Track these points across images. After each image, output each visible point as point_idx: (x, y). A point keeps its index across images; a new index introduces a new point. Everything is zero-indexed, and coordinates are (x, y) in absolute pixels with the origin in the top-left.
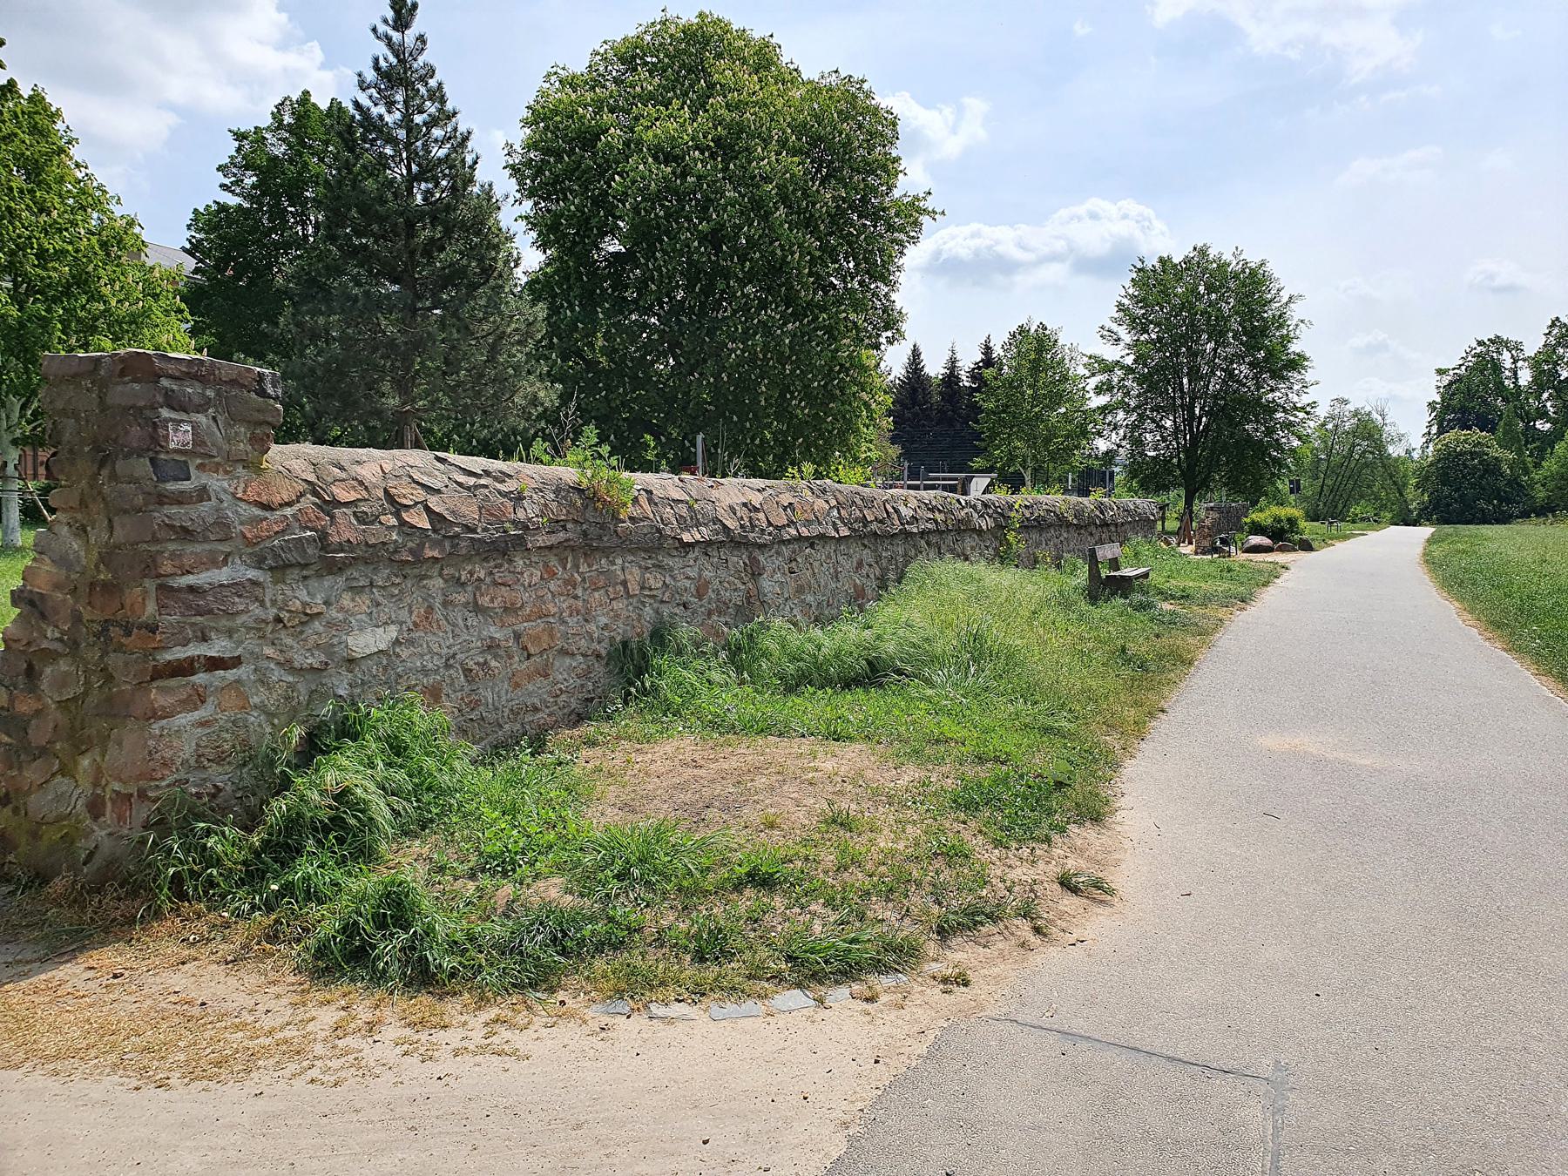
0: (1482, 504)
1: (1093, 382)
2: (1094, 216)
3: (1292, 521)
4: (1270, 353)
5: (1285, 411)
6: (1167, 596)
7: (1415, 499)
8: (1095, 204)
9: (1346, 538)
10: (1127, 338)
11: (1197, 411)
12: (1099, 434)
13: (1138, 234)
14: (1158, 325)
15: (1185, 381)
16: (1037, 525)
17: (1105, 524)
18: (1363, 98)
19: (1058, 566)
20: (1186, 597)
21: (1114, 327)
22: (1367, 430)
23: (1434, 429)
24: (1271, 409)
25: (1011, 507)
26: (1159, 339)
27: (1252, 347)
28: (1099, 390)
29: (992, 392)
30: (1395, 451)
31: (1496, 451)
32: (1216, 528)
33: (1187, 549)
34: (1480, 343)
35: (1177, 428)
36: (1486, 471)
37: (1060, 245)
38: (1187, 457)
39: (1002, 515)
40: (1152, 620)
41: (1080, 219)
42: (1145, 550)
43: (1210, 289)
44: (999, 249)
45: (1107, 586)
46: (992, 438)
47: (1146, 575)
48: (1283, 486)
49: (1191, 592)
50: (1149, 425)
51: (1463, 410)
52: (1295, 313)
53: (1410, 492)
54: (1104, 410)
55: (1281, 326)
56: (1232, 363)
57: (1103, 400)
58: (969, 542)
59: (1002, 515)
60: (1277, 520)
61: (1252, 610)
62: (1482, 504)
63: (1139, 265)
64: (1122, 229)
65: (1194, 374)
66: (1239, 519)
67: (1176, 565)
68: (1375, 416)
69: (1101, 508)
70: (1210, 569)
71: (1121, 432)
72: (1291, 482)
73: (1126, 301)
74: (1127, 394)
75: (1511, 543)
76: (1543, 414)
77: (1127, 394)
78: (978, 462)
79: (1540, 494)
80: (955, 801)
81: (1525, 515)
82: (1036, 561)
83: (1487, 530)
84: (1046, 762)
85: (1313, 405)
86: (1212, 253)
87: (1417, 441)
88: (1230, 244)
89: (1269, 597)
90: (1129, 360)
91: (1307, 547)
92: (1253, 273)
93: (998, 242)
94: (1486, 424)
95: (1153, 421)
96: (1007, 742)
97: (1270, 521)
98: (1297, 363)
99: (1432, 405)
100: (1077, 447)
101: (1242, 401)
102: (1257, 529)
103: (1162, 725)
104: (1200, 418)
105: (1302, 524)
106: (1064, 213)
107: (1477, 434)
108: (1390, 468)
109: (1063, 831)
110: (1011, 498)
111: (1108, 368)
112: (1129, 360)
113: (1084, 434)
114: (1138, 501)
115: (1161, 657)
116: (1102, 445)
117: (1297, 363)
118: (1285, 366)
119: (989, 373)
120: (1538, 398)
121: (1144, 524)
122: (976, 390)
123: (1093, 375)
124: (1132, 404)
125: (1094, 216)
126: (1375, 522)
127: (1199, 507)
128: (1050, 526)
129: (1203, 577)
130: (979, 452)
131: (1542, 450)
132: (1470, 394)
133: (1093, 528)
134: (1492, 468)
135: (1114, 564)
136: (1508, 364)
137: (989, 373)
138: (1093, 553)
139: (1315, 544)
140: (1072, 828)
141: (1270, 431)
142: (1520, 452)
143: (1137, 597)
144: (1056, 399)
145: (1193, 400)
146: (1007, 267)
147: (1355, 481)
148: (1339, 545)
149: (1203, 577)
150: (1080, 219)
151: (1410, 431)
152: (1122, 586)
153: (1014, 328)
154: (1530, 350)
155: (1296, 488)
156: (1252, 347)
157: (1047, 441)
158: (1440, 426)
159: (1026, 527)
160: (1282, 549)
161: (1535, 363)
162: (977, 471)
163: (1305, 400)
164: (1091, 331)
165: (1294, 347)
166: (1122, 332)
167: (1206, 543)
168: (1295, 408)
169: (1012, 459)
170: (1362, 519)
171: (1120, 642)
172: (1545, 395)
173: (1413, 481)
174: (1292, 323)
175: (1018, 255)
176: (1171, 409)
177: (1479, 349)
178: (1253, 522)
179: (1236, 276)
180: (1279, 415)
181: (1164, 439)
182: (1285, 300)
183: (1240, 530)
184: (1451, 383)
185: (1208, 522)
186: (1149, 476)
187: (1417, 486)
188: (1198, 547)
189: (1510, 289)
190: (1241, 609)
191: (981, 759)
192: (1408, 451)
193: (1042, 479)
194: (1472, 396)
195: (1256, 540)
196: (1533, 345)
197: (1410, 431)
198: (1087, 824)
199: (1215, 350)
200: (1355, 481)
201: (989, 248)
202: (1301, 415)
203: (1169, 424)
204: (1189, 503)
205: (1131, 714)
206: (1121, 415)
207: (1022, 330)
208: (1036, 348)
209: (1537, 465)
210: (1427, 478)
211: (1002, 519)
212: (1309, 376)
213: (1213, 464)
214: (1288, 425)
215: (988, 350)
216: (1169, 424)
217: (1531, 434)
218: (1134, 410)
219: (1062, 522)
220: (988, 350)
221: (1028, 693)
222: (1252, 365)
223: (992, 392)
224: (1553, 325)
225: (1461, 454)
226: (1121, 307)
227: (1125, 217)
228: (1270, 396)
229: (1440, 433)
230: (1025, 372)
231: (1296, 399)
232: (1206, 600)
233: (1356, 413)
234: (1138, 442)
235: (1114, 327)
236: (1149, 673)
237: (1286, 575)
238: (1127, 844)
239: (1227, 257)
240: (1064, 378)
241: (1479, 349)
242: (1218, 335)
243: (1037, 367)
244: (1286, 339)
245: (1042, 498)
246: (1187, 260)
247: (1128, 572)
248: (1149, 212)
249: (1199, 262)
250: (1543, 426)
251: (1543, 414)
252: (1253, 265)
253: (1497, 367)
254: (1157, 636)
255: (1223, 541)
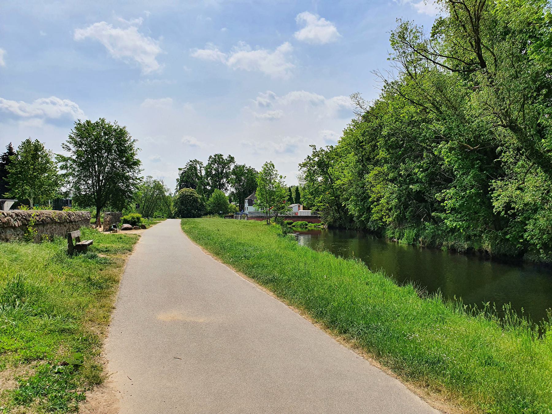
0: (193, 211)
1: (60, 164)
2: (54, 103)
3: (138, 218)
4: (128, 159)
5: (133, 179)
6: (101, 251)
7: (173, 210)
8: (54, 99)
9: (155, 223)
10: (74, 149)
11: (101, 178)
12: (62, 185)
13: (72, 112)
14: (86, 145)
15: (96, 166)
16: (42, 223)
17: (71, 222)
18: (148, 80)
19: (52, 241)
20: (107, 251)
21: (68, 144)
22: (158, 187)
23: (178, 188)
24: (127, 178)
25: (30, 216)
26: (86, 151)
27: (121, 156)
28: (62, 168)
29: (13, 165)
30: (167, 194)
31: (196, 195)
32: (111, 222)
33: (101, 229)
34: (191, 161)
35: (93, 183)
36: (194, 201)
37: (40, 112)
38: (97, 195)
39: (25, 219)
40: (97, 263)
41: (47, 103)
42: (87, 231)
43: (105, 134)
44: (12, 109)
45: (76, 249)
46: (14, 185)
47: (91, 243)
48: (133, 205)
49: (110, 248)
50: (82, 182)
51: (187, 182)
52: (135, 146)
53: (172, 208)
54: (64, 175)
55: (131, 150)
56: (114, 161)
57: (64, 172)
58: (9, 233)
59: (25, 219)
60: (133, 218)
61: (134, 254)
62: (193, 211)
63: (78, 122)
64: (65, 109)
65: (100, 164)
66: (119, 218)
67: (96, 236)
68: (160, 182)
69: (69, 215)
70: (113, 239)
71: (71, 184)
72: (136, 204)
73: (73, 135)
74: (74, 170)
75: (208, 223)
76: (208, 184)
77: (74, 170)
78: (7, 195)
79: (209, 208)
80: (16, 399)
81: (206, 214)
82: (42, 239)
83: (197, 220)
84: (63, 352)
85: (143, 178)
86: (106, 122)
87: (173, 191)
88: (114, 120)
89: (137, 248)
90: (74, 157)
91: (144, 227)
92: (121, 130)
93: (10, 106)
94: (193, 186)
95: (84, 181)
96: (41, 345)
97: (130, 218)
98: (137, 163)
99: (177, 180)
100: (53, 190)
101: (118, 174)
102: (126, 221)
103: (115, 315)
104: (102, 180)
105: (142, 219)
106: (39, 101)
107: (191, 190)
108: (166, 200)
109: (83, 398)
110: (30, 212)
111: (65, 159)
112: (74, 157)
113: (57, 185)
114: (83, 212)
115: (106, 280)
116: (64, 190)
117: (137, 163)
118: (132, 164)
119: (12, 157)
120: (207, 179)
121: (86, 221)
122: (5, 164)
123: (59, 162)
124: (76, 174)
125: (54, 103)
126: (162, 218)
127: (102, 214)
128: (48, 223)
129: (112, 242)
130: (8, 190)
131: (208, 195)
132: (188, 177)
133: (66, 224)
134: (195, 200)
135: (78, 239)
136: (199, 168)
137: (12, 157)
138: (70, 235)
139: (147, 226)
140: (88, 394)
141: (128, 186)
142: (203, 195)
143: (89, 253)
144: (44, 170)
145: (99, 174)
146: (17, 118)
147: (154, 205)
148: (154, 226)
149: (112, 242)
150: (47, 103)
151: (171, 188)
152: (83, 248)
153: (24, 141)
154: (205, 165)
155: (138, 206)
156: (121, 156)
157: (40, 187)
158: (180, 186)
159: (37, 225)
160: (135, 229)
161: (206, 169)
162: (7, 198)
163: (139, 176)
164: (58, 146)
165: (136, 157)
166: (71, 146)
167: (107, 227)
168: (136, 179)
169: (24, 193)
170: (158, 217)
171: (87, 276)
172: (209, 179)
173: (173, 204)
174: (135, 149)
175: (21, 113)
176: (91, 176)
177: (191, 163)
178: (124, 219)
179: (115, 131)
180: (131, 181)
181: (89, 188)
182: (132, 141)
183: (120, 222)
184: (183, 173)
185: (108, 219)
186: (82, 201)
187: (174, 206)
188: (104, 229)
189: (194, 146)
190: (130, 254)
191: (28, 360)
192: (170, 194)
193: (37, 203)
194: (188, 178)
195: (126, 225)
196: (205, 163)
197: (171, 188)
198: (95, 388)
199: (107, 156)
200: (154, 205)
201: (7, 109)
202: (139, 181)
203: (90, 182)
204: (98, 212)
205: (101, 313)
206: (71, 178)
207: (28, 141)
208: (33, 150)
209: (208, 200)
210: (177, 203)
211: (25, 221)
212: (141, 167)
213: (107, 198)
214: (133, 184)
215: (10, 149)
216: (90, 182)
217: (205, 190)
218: (76, 176)
219: (53, 221)
220: (10, 149)
221: (50, 311)
222: (121, 163)
223: (13, 165)
224: (210, 158)
225: (187, 195)
226: (71, 137)
227: (67, 105)
228: (127, 174)
229: (180, 189)
230: (29, 158)
231: (136, 175)
232: (116, 252)
233: (155, 181)
234: (78, 189)
235: (68, 144)
236: (102, 288)
237: (141, 239)
238: (118, 396)
239: (112, 124)
240: (48, 162)
241: (191, 163)
242: (109, 151)
243: (35, 157)
244: (133, 155)
245: (44, 211)
246: (97, 123)
247: (84, 242)
248: (77, 106)
249: (101, 125)
250: (209, 188)
251: (208, 184)
252: (121, 127)
253: (196, 169)
254: (101, 270)
255: (115, 227)
